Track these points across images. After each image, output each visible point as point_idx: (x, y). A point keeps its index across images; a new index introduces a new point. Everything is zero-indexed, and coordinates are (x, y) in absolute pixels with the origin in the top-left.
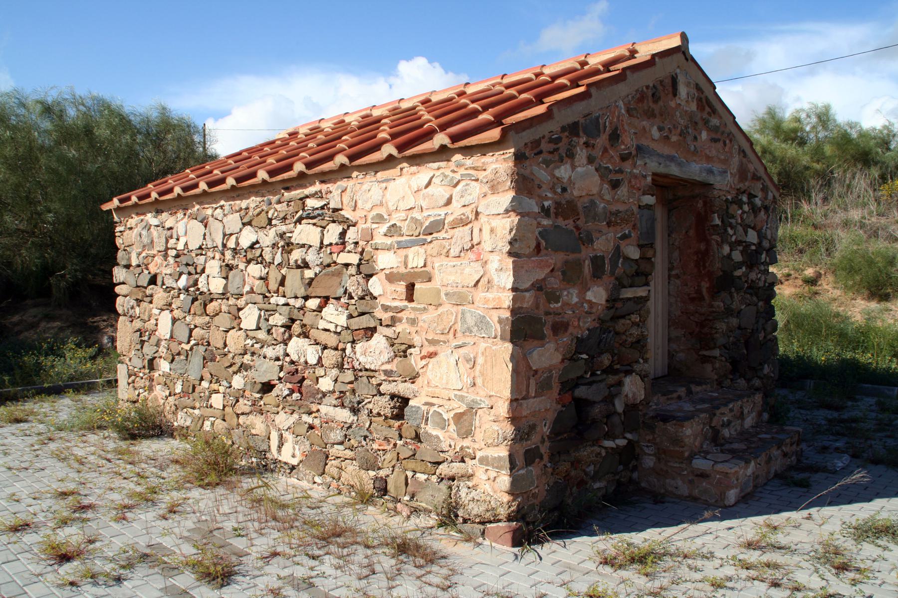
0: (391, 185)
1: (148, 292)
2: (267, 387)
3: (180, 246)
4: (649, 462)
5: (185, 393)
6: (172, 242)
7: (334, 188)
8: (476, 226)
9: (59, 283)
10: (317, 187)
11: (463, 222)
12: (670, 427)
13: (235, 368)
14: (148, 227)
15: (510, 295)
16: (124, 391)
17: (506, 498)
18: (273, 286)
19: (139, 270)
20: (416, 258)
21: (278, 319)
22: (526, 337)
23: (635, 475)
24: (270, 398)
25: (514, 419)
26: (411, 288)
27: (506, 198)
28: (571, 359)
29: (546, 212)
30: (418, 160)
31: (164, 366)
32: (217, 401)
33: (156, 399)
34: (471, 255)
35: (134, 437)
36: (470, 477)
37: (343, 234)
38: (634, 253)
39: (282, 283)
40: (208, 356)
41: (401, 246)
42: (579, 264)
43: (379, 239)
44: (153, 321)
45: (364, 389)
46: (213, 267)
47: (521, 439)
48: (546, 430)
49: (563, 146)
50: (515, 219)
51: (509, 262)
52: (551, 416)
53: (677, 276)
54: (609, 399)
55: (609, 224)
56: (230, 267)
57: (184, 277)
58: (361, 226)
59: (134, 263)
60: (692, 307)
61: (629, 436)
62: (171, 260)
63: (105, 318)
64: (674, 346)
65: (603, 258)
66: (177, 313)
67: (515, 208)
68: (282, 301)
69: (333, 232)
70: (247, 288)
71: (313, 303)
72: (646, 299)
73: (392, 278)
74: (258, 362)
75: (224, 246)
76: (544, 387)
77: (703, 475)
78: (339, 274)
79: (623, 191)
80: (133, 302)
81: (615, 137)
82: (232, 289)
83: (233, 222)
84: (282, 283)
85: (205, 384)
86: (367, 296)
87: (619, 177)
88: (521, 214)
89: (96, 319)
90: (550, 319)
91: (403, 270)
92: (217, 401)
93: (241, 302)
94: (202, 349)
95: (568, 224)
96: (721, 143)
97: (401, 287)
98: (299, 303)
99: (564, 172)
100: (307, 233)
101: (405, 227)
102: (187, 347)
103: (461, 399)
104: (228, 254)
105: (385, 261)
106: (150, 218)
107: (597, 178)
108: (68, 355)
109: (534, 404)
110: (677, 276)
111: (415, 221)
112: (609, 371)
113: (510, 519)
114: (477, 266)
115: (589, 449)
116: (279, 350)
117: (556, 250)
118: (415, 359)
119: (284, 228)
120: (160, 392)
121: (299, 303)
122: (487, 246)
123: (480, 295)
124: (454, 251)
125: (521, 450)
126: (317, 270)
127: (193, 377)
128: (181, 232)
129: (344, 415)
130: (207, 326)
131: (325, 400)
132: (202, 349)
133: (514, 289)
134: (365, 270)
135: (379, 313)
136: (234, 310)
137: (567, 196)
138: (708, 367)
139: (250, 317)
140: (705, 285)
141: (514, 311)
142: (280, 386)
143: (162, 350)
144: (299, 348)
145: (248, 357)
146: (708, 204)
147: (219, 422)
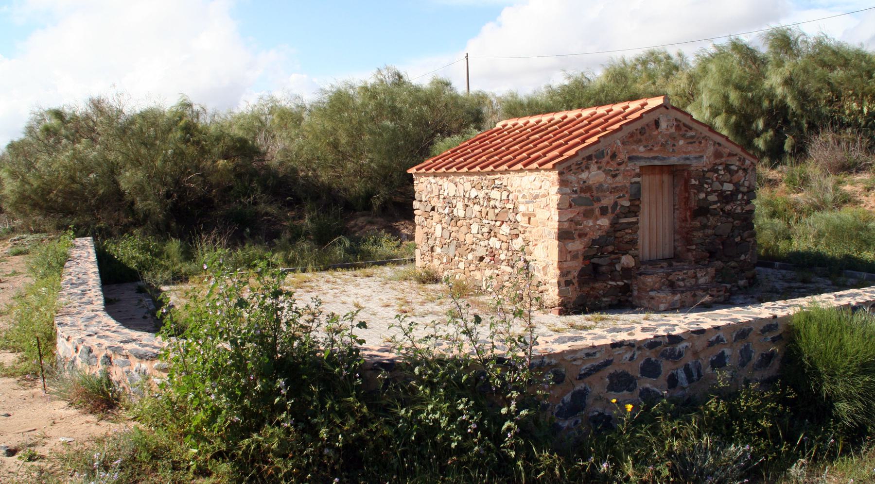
0: (523, 179)
1: (431, 214)
2: (481, 259)
3: (445, 194)
4: (635, 293)
5: (448, 262)
6: (441, 192)
7: (505, 176)
8: (548, 197)
9: (377, 202)
10: (498, 176)
11: (544, 196)
12: (642, 278)
13: (469, 251)
14: (430, 183)
15: (557, 223)
16: (419, 263)
17: (558, 298)
18: (484, 215)
19: (426, 203)
20: (531, 207)
21: (486, 230)
22: (565, 239)
23: (630, 299)
24: (483, 263)
25: (560, 268)
26: (529, 219)
27: (556, 188)
28: (589, 247)
29: (575, 192)
30: (530, 170)
31: (438, 250)
32: (461, 265)
33: (434, 266)
34: (547, 208)
35: (424, 283)
36: (547, 290)
37: (508, 196)
38: (627, 203)
39: (487, 214)
40: (458, 245)
41: (527, 203)
42: (592, 211)
43: (520, 199)
44: (433, 229)
45: (515, 258)
46: (460, 205)
47: (563, 276)
48: (576, 274)
49: (583, 166)
50: (559, 196)
51: (557, 212)
52: (579, 269)
53: (677, 209)
54: (612, 264)
55: (611, 193)
56: (467, 206)
57: (447, 209)
58: (514, 193)
59: (424, 200)
60: (683, 225)
61: (626, 281)
62: (441, 200)
63: (403, 223)
64: (676, 243)
65: (607, 207)
66: (444, 225)
67: (560, 191)
68: (487, 222)
69: (505, 194)
70: (473, 216)
71: (498, 223)
72: (637, 223)
73: (524, 215)
74: (478, 248)
75: (464, 196)
76: (575, 257)
77: (652, 298)
78: (507, 212)
79: (619, 178)
80: (423, 219)
81: (614, 156)
82: (468, 216)
83: (468, 186)
84: (487, 214)
85: (456, 258)
86: (516, 221)
87: (617, 172)
88: (562, 194)
89: (398, 224)
90: (577, 232)
91: (527, 212)
92: (461, 265)
93: (471, 222)
94: (455, 242)
95: (588, 195)
96: (697, 143)
97: (526, 219)
98: (493, 223)
99: (584, 176)
100: (495, 194)
101: (527, 195)
102: (449, 241)
103: (544, 261)
104: (466, 200)
105: (522, 208)
106: (431, 178)
107: (603, 175)
108: (384, 245)
109: (570, 264)
110: (677, 209)
111: (531, 194)
112: (612, 253)
113: (559, 306)
114: (548, 212)
115: (600, 284)
116: (486, 242)
117: (580, 205)
118: (531, 247)
119: (487, 191)
120: (436, 262)
121: (493, 223)
122: (551, 205)
123: (549, 223)
124: (542, 207)
125: (563, 280)
126: (499, 209)
127: (451, 255)
128: (446, 188)
129: (509, 269)
130: (458, 231)
131: (503, 263)
132: (455, 242)
133: (559, 221)
134: (515, 211)
135: (520, 229)
136: (468, 225)
137: (586, 184)
138: (690, 254)
139: (475, 228)
140: (688, 214)
141: (559, 229)
142: (486, 258)
143: (438, 243)
144: (494, 242)
145: (474, 245)
146: (689, 173)
147: (462, 275)
